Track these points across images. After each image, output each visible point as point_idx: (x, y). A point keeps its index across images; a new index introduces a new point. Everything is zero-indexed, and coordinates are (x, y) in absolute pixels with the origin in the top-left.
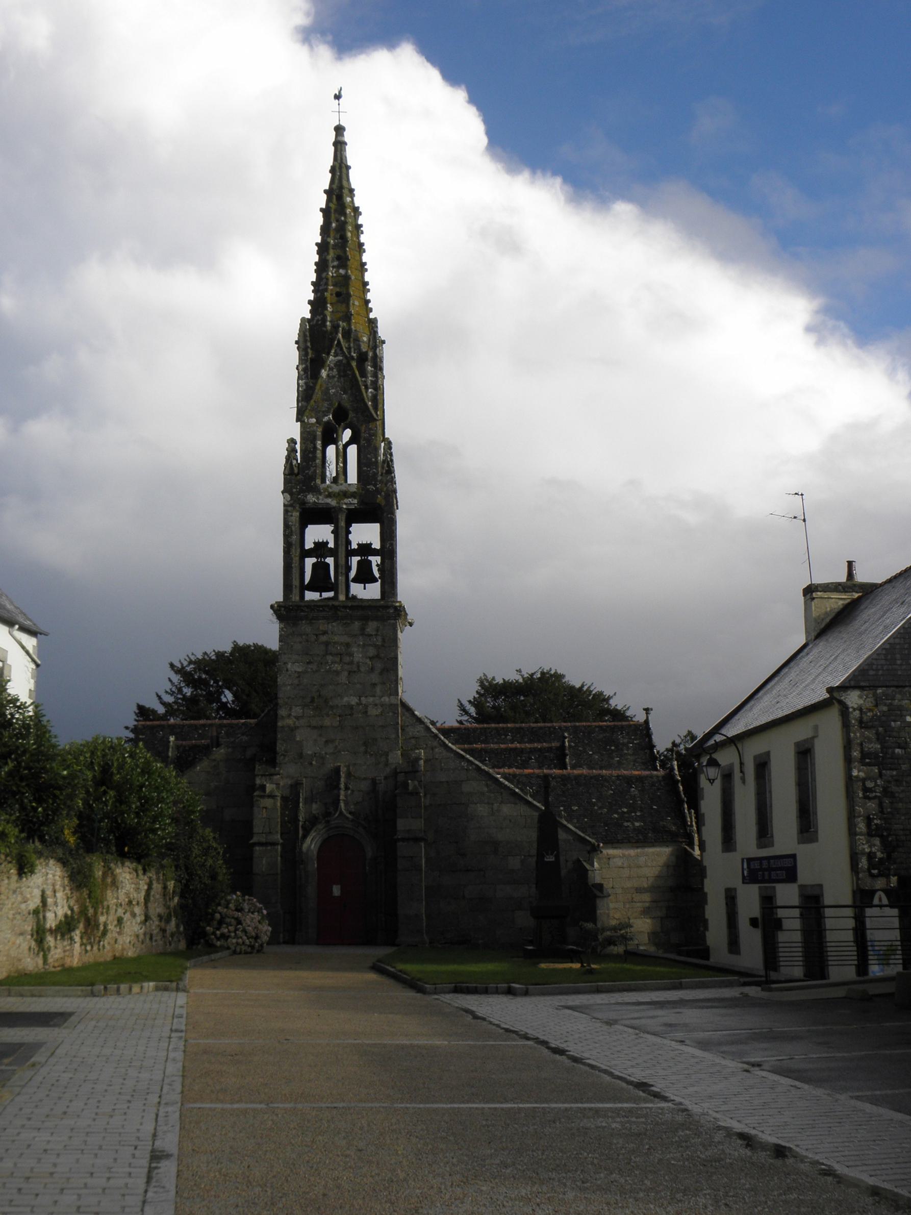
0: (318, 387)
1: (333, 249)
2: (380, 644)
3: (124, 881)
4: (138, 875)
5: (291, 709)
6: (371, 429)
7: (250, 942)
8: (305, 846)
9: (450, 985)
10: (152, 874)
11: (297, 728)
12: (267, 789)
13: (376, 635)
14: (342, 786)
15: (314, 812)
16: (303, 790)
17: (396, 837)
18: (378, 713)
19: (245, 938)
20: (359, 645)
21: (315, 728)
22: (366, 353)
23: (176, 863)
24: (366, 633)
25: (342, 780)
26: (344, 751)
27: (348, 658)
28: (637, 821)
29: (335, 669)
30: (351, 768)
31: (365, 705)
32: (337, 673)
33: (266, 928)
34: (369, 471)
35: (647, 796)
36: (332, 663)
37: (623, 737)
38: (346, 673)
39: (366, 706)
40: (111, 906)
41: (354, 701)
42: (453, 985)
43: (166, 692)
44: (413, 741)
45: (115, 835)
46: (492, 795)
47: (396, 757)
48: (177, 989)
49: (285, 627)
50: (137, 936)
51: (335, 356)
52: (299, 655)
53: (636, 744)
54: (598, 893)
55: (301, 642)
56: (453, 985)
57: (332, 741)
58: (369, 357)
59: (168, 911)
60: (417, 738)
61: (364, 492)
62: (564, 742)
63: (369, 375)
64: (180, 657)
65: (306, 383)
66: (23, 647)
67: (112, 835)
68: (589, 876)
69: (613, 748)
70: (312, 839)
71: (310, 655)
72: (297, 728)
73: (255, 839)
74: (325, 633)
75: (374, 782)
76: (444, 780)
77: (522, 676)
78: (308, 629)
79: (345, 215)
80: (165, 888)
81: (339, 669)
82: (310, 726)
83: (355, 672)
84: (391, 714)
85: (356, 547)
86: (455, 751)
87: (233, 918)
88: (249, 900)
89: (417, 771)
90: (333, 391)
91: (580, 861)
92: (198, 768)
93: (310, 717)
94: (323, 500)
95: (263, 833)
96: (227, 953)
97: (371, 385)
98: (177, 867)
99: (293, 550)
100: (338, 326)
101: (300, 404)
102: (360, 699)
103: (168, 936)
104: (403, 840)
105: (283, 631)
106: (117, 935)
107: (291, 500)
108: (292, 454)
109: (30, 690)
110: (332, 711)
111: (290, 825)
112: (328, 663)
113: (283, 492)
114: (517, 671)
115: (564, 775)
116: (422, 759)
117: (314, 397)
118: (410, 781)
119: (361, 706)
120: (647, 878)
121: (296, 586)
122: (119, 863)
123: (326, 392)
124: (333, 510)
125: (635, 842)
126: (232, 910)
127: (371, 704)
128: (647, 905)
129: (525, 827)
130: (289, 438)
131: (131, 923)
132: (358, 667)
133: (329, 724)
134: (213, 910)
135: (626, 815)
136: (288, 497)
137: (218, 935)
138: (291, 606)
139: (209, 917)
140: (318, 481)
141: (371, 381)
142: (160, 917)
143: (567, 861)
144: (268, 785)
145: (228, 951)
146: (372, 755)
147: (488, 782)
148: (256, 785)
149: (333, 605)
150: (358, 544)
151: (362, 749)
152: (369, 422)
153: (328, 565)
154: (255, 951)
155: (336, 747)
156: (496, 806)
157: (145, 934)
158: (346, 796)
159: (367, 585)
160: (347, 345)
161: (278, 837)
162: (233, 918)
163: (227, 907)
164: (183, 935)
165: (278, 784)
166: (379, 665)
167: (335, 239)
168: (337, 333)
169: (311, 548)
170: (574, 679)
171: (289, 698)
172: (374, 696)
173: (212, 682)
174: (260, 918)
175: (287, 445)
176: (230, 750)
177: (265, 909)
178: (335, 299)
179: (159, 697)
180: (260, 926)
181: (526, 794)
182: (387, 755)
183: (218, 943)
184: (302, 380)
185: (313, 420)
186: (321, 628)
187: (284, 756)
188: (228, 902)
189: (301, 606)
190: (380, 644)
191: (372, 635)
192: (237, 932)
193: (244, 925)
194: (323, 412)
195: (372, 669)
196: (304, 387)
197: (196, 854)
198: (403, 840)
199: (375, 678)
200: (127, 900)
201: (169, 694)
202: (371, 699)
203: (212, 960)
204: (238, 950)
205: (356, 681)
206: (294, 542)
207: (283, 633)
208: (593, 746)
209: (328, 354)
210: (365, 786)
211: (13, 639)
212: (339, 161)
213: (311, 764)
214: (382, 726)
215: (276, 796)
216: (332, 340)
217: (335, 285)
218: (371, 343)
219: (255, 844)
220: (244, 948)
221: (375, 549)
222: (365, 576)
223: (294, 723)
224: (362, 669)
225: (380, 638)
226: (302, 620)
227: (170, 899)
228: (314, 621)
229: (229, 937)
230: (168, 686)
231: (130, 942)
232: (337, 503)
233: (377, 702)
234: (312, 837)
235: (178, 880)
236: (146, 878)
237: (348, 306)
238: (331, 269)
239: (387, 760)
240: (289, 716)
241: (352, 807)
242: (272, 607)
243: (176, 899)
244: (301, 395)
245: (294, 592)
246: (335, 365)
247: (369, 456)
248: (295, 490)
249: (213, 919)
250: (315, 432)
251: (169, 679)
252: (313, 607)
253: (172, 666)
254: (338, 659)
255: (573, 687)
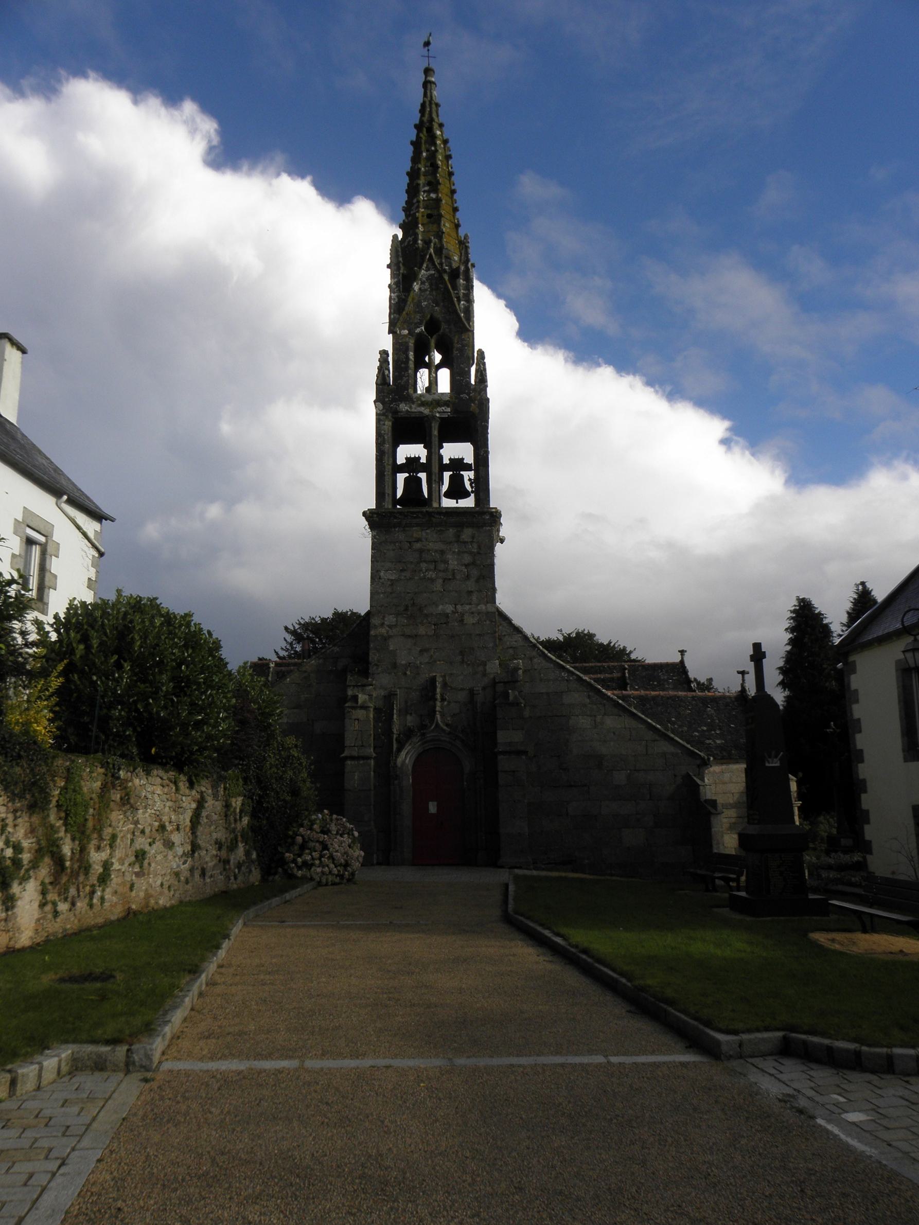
0: (410, 299)
1: (424, 176)
2: (475, 551)
3: (150, 796)
4: (177, 789)
5: (384, 617)
6: (463, 340)
7: (339, 871)
8: (399, 760)
9: (766, 1035)
10: (205, 786)
11: (390, 637)
12: (359, 700)
13: (472, 542)
14: (438, 696)
15: (409, 724)
16: (397, 701)
17: (496, 750)
18: (474, 622)
19: (332, 866)
20: (454, 552)
21: (409, 636)
22: (458, 268)
23: (244, 774)
24: (462, 540)
25: (438, 690)
26: (439, 661)
27: (443, 565)
28: (718, 739)
29: (429, 576)
30: (447, 679)
31: (461, 613)
32: (432, 580)
33: (358, 853)
34: (463, 380)
35: (723, 716)
36: (426, 571)
37: (663, 674)
38: (440, 581)
39: (462, 615)
40: (120, 835)
41: (449, 609)
42: (780, 1034)
43: (282, 649)
44: (511, 651)
45: (135, 730)
46: (595, 707)
47: (494, 667)
48: (129, 1066)
49: (377, 535)
50: (177, 874)
51: (426, 271)
52: (392, 562)
53: (674, 680)
54: (713, 811)
55: (394, 550)
56: (780, 1034)
57: (427, 650)
58: (461, 271)
59: (232, 836)
60: (514, 648)
61: (457, 401)
62: (624, 674)
63: (461, 288)
64: (292, 621)
65: (398, 296)
66: (85, 535)
67: (131, 729)
68: (701, 791)
69: (655, 683)
70: (407, 752)
71: (404, 562)
72: (390, 637)
73: (346, 753)
74: (418, 540)
75: (472, 692)
76: (544, 691)
77: (563, 635)
78: (401, 536)
79: (435, 144)
80: (227, 806)
81: (433, 576)
82: (403, 635)
83: (450, 579)
84: (488, 622)
85: (448, 462)
86: (555, 661)
87: (318, 841)
88: (337, 819)
89: (517, 681)
90: (425, 303)
91: (689, 776)
92: (288, 680)
93: (403, 626)
94: (415, 409)
95: (354, 746)
96: (308, 887)
97: (463, 297)
98: (246, 780)
99: (386, 458)
100: (430, 241)
101: (392, 316)
102: (455, 607)
103: (232, 867)
104: (504, 753)
105: (376, 538)
106: (134, 877)
107: (383, 409)
108: (384, 365)
109: (89, 579)
110: (427, 619)
111: (383, 737)
112: (422, 570)
113: (375, 402)
114: (558, 630)
115: (642, 696)
116: (521, 669)
117: (406, 309)
118: (510, 691)
119: (457, 615)
120: (733, 794)
121: (388, 494)
122: (139, 770)
123: (418, 304)
124: (426, 419)
125: (721, 759)
126: (317, 833)
127: (467, 612)
128: (733, 820)
129: (630, 739)
130: (381, 349)
131: (165, 856)
132: (454, 574)
133: (424, 633)
134: (294, 831)
135: (707, 733)
136: (381, 406)
137: (300, 864)
138: (384, 512)
139: (289, 840)
140: (411, 391)
141: (463, 293)
142: (219, 845)
143: (675, 776)
144: (360, 696)
145: (313, 883)
146: (469, 665)
147: (590, 694)
148: (348, 696)
149: (426, 511)
150: (450, 459)
151: (459, 658)
152: (462, 333)
153: (420, 479)
154: (345, 881)
155: (431, 656)
156: (599, 718)
157: (192, 870)
158: (442, 707)
159: (459, 500)
160: (438, 261)
161: (371, 751)
162: (318, 841)
163: (311, 829)
164: (257, 863)
165: (370, 695)
166: (475, 572)
167: (425, 167)
168: (428, 248)
169: (403, 464)
170: (603, 638)
171: (382, 606)
172: (470, 604)
173: (317, 640)
174: (350, 841)
175: (379, 356)
176: (321, 661)
177: (356, 831)
178: (426, 220)
179: (277, 653)
180: (350, 851)
181: (630, 705)
182: (486, 665)
183: (300, 873)
184: (394, 293)
185: (406, 332)
186: (415, 535)
187: (376, 665)
188: (312, 823)
189: (394, 513)
190: (475, 551)
191: (467, 542)
192: (323, 859)
193: (331, 849)
194: (416, 324)
195: (468, 577)
196: (397, 300)
197: (271, 763)
198: (504, 753)
199: (471, 585)
200: (157, 824)
201: (284, 650)
202: (467, 607)
203: (286, 902)
204: (324, 881)
205: (451, 589)
206: (386, 450)
207: (375, 540)
208: (638, 682)
209: (420, 268)
210: (462, 696)
211: (67, 518)
212: (429, 99)
213: (405, 674)
214: (480, 635)
215: (369, 707)
216: (423, 258)
217: (426, 208)
218: (463, 257)
219: (346, 758)
220: (330, 878)
221: (467, 463)
222: (457, 491)
223: (388, 632)
224: (458, 577)
225: (475, 546)
226: (395, 527)
227: (235, 820)
228: (407, 529)
229: (312, 865)
230: (284, 644)
231: (162, 885)
232: (430, 411)
233: (474, 610)
234: (406, 751)
235: (248, 796)
236: (194, 792)
237: (439, 225)
238: (422, 193)
239: (485, 670)
240: (382, 625)
241: (449, 719)
242: (364, 514)
243: (246, 820)
244: (393, 307)
245: (387, 500)
246: (427, 279)
247: (462, 365)
248: (387, 399)
249: (293, 843)
250: (407, 343)
251: (284, 638)
252: (406, 514)
253: (286, 628)
254: (432, 567)
255: (602, 644)
